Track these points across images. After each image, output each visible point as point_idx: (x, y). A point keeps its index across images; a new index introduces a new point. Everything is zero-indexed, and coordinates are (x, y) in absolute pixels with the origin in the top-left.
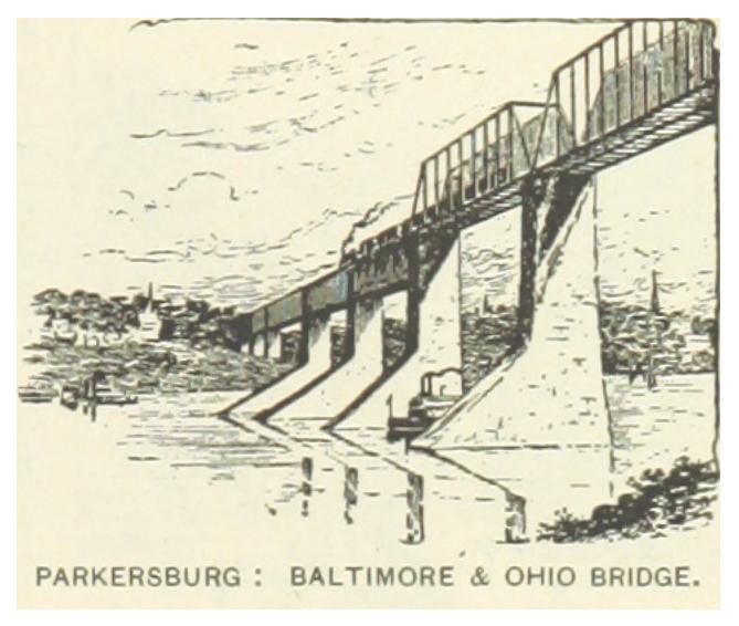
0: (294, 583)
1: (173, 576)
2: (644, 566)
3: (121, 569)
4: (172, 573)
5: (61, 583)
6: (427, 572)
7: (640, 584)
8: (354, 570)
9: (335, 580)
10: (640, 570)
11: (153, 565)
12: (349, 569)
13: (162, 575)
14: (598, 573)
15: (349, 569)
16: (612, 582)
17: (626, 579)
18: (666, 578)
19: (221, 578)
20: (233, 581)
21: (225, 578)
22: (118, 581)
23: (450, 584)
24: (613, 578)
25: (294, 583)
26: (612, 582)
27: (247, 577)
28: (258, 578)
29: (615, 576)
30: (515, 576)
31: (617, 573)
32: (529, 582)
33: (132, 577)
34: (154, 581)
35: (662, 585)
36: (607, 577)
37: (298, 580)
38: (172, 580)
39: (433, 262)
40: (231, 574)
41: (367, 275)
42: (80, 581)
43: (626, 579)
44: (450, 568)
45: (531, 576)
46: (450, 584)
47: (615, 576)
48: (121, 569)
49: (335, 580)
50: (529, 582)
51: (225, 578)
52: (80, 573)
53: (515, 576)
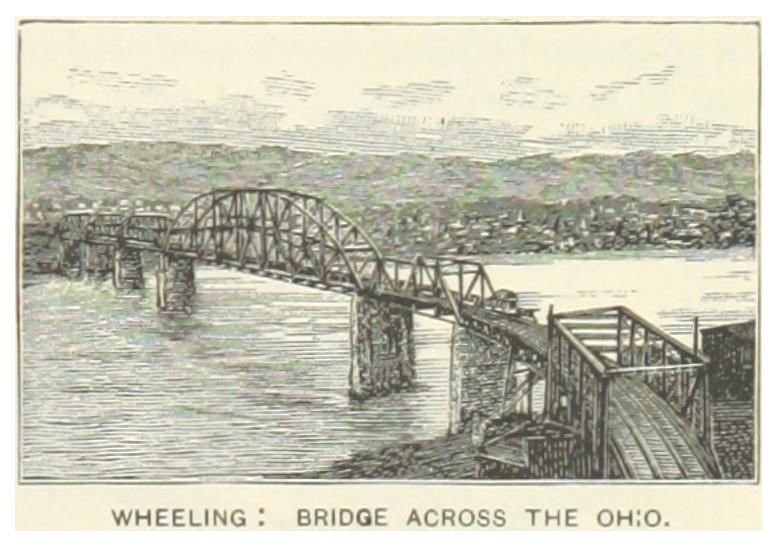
0: (300, 524)
1: (305, 517)
2: (344, 507)
3: (165, 510)
4: (304, 514)
5: (414, 524)
6: (449, 514)
7: (342, 524)
8: (533, 512)
9: (195, 521)
10: (342, 511)
11: (484, 508)
12: (528, 511)
13: (491, 517)
14: (304, 514)
15: (528, 511)
16: (316, 523)
17: (329, 519)
18: (241, 519)
19: (456, 519)
20: (239, 522)
21: (460, 519)
22: (161, 521)
23: (385, 524)
24: (317, 518)
25: (300, 524)
26: (316, 523)
27: (252, 517)
28: (261, 517)
29: (320, 517)
30: (606, 518)
31: (321, 514)
32: (619, 523)
33: (445, 518)
34: (484, 522)
35: (237, 525)
36: (312, 517)
37: (304, 521)
38: (304, 521)
39: (686, 209)
40: (238, 516)
41: (672, 230)
42: (321, 522)
43: (329, 519)
44: (383, 510)
45: (620, 518)
46: (385, 524)
47: (320, 517)
48: (165, 510)
49: (195, 521)
50: (619, 523)
51: (460, 519)
52: (449, 514)
53: (606, 518)
